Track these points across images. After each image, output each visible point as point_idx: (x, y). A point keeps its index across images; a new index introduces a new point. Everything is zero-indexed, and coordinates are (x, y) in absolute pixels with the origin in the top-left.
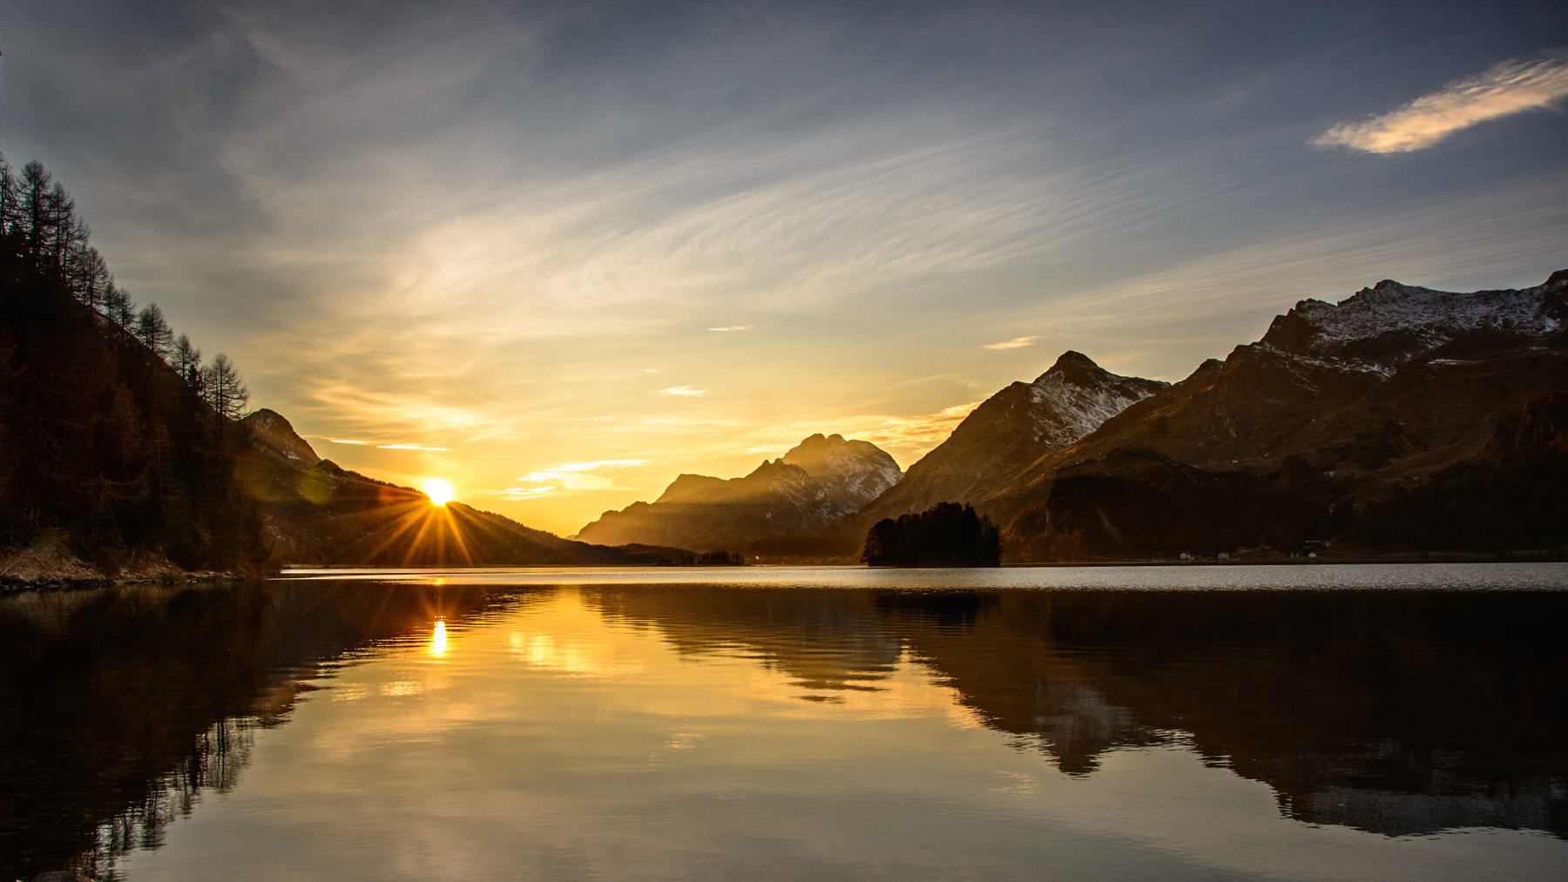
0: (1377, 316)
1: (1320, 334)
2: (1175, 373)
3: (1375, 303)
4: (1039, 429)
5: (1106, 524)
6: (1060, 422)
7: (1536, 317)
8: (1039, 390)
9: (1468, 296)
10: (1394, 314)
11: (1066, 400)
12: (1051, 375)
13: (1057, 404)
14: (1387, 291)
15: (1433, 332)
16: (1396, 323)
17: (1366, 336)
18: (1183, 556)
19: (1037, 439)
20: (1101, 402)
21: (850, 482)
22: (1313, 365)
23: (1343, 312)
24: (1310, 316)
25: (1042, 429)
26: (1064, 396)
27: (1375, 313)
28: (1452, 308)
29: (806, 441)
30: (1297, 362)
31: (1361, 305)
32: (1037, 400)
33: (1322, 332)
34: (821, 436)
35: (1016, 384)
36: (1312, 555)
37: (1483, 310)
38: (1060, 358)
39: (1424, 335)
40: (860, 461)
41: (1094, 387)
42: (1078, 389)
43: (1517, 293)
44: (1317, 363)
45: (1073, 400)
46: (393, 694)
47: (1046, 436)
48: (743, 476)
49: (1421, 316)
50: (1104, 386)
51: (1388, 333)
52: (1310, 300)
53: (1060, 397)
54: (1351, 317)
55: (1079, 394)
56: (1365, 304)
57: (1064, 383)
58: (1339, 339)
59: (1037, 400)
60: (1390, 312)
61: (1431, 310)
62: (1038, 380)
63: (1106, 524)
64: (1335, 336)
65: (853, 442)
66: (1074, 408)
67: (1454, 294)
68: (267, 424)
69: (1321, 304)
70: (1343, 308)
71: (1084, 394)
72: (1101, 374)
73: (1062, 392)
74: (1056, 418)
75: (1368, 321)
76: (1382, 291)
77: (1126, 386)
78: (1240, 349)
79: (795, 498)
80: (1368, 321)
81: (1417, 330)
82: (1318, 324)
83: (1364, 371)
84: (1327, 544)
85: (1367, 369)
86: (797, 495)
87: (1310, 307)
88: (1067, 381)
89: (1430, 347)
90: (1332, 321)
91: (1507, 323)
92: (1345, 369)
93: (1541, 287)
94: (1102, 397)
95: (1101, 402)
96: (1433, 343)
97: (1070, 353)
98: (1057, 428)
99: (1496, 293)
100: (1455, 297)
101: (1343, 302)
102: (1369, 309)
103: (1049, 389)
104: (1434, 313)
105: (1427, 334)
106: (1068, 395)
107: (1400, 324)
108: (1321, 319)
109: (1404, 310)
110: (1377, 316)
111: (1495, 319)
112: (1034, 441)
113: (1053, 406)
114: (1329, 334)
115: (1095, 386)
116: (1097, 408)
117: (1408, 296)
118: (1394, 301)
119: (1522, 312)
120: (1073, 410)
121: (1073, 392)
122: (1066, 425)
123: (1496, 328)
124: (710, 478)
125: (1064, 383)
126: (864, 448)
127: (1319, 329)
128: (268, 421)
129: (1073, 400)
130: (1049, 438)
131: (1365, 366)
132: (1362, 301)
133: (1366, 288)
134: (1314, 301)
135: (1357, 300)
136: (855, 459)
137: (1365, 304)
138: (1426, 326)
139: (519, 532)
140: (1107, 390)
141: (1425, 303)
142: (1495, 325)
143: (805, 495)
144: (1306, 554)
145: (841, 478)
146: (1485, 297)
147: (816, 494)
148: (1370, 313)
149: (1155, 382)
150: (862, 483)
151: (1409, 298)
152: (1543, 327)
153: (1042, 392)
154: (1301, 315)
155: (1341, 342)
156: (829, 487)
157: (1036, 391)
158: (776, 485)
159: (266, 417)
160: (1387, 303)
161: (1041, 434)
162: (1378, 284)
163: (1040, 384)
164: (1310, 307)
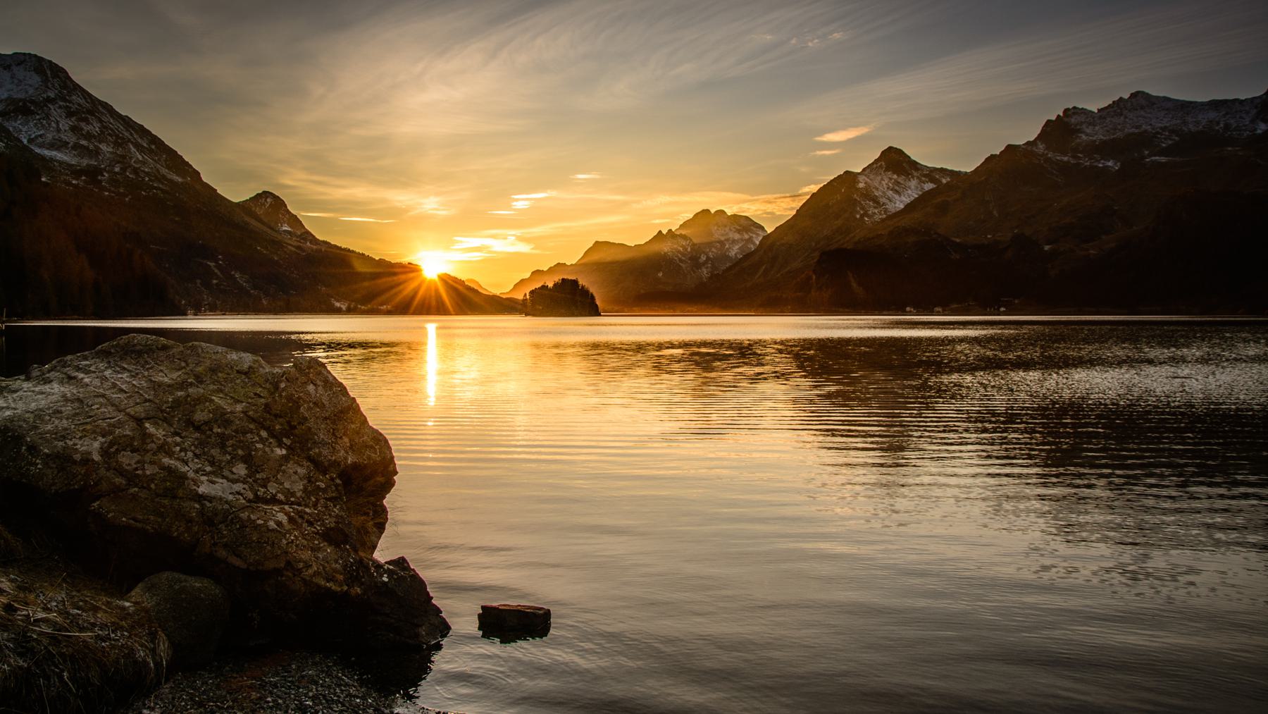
0: (1127, 120)
1: (1080, 135)
2: (968, 168)
3: (1127, 109)
4: (860, 208)
5: (854, 285)
6: (878, 203)
7: (1252, 121)
8: (864, 177)
9: (1202, 104)
10: (1140, 118)
11: (885, 185)
12: (875, 166)
13: (877, 189)
14: (1140, 100)
15: (1167, 133)
16: (1141, 126)
17: (1115, 136)
18: (908, 309)
19: (858, 216)
20: (913, 187)
21: (730, 248)
22: (1061, 161)
23: (1100, 117)
25: (863, 208)
26: (883, 182)
28: (1188, 114)
29: (696, 215)
30: (1050, 158)
31: (1115, 111)
32: (861, 185)
33: (1081, 133)
34: (708, 211)
35: (847, 172)
36: (1002, 309)
37: (1212, 115)
38: (883, 152)
39: (1159, 136)
40: (739, 231)
41: (908, 175)
42: (895, 176)
43: (1241, 102)
44: (1066, 159)
45: (890, 185)
46: (140, 585)
47: (866, 214)
48: (643, 243)
49: (1162, 120)
50: (915, 174)
51: (1133, 134)
52: (1074, 108)
53: (880, 183)
54: (1107, 121)
55: (896, 181)
56: (1119, 111)
57: (884, 171)
58: (1094, 138)
59: (861, 185)
60: (1137, 117)
61: (1171, 116)
62: (864, 170)
63: (854, 285)
64: (1091, 136)
65: (735, 216)
66: (891, 192)
67: (1191, 103)
68: (267, 203)
70: (1100, 114)
71: (899, 181)
72: (915, 165)
73: (882, 179)
74: (875, 200)
75: (1119, 124)
76: (1133, 100)
77: (932, 174)
78: (1009, 147)
79: (681, 260)
80: (1119, 124)
81: (1154, 131)
82: (1078, 127)
83: (1101, 165)
84: (1016, 301)
85: (1103, 164)
86: (683, 258)
87: (1074, 113)
88: (887, 170)
89: (1164, 145)
90: (1090, 124)
91: (1227, 127)
92: (1086, 164)
93: (1260, 97)
94: (913, 183)
95: (913, 187)
96: (1166, 142)
97: (890, 148)
98: (875, 208)
99: (1225, 102)
100: (1192, 105)
101: (1102, 109)
102: (1121, 115)
103: (872, 177)
104: (1172, 118)
105: (1162, 135)
106: (886, 182)
107: (1144, 126)
108: (1082, 122)
109: (1149, 115)
110: (1127, 120)
111: (1218, 123)
112: (856, 219)
114: (1087, 135)
115: (909, 174)
116: (910, 192)
117: (1155, 104)
118: (1142, 108)
119: (1241, 117)
120: (890, 193)
121: (891, 179)
122: (883, 205)
123: (1218, 130)
124: (619, 244)
125: (884, 171)
126: (742, 222)
127: (1079, 131)
128: (268, 200)
129: (890, 185)
130: (868, 216)
131: (1102, 161)
132: (1116, 108)
133: (1121, 98)
134: (1078, 108)
135: (1113, 107)
136: (734, 230)
137: (1119, 111)
139: (756, 213)
140: (918, 178)
141: (1167, 110)
142: (1217, 128)
143: (690, 259)
144: (998, 309)
145: (721, 242)
146: (1215, 105)
147: (700, 258)
148: (1122, 118)
149: (956, 172)
150: (740, 248)
151: (1155, 106)
152: (1256, 130)
153: (866, 179)
154: (1066, 119)
155: (1095, 141)
156: (713, 252)
157: (861, 178)
158: (666, 247)
159: (267, 197)
160: (1137, 110)
162: (1132, 94)
163: (866, 172)
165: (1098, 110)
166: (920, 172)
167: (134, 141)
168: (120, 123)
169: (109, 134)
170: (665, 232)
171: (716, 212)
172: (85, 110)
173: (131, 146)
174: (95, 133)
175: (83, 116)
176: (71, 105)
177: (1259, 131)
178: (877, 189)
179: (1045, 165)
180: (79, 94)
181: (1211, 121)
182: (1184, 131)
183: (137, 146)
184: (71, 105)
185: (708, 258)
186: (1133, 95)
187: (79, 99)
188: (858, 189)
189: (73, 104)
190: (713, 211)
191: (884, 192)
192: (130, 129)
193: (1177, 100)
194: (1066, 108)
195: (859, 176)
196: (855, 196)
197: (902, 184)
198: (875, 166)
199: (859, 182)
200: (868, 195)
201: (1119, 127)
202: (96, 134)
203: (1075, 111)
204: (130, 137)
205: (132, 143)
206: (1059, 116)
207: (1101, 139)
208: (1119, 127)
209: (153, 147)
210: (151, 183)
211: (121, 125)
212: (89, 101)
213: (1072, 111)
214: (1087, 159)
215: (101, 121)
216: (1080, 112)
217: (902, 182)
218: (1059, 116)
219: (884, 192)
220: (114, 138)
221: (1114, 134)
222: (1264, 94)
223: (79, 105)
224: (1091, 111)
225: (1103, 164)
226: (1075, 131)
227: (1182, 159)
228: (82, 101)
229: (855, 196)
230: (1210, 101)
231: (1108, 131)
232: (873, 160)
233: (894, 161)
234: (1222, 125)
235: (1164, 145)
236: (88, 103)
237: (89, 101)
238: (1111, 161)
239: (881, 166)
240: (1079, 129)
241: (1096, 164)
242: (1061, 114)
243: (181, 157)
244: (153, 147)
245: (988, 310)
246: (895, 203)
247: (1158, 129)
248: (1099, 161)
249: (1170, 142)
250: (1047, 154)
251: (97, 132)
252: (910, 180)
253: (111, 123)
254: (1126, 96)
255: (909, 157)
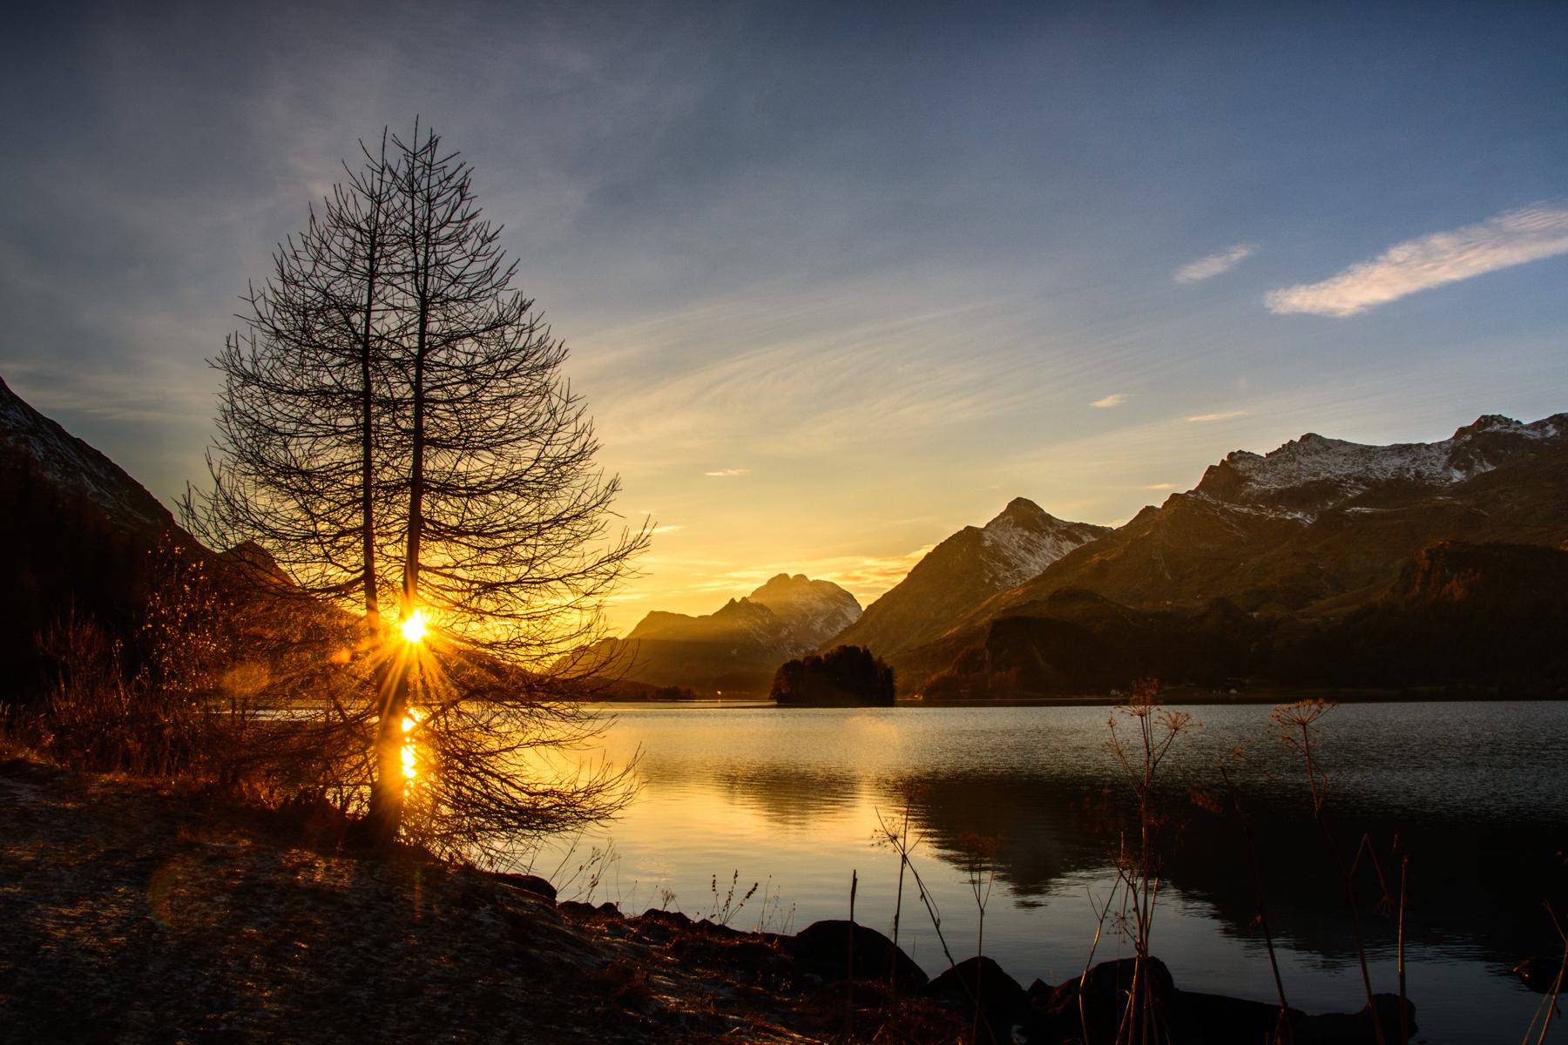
0: (1302, 466)
1: (1250, 483)
6: (1009, 564)
7: (1445, 469)
8: (989, 533)
9: (1384, 449)
12: (1001, 521)
15: (1352, 482)
16: (1319, 473)
19: (987, 581)
20: (1048, 546)
22: (1241, 513)
24: (1240, 466)
27: (1300, 463)
28: (1370, 460)
31: (1287, 456)
32: (987, 543)
33: (1251, 481)
34: (785, 576)
37: (1397, 461)
39: (1344, 485)
41: (1042, 532)
42: (1027, 533)
43: (1428, 447)
44: (1245, 510)
47: (995, 578)
49: (1342, 467)
50: (1050, 530)
51: (1311, 482)
52: (1240, 452)
55: (1028, 538)
57: (1013, 527)
58: (1267, 488)
59: (987, 543)
60: (1313, 463)
62: (988, 525)
66: (1023, 551)
67: (1371, 447)
69: (1250, 456)
70: (1270, 459)
71: (1032, 538)
72: (1049, 519)
73: (1012, 537)
75: (1293, 471)
79: (760, 636)
82: (1247, 474)
83: (1288, 518)
84: (1247, 681)
85: (1291, 516)
86: (762, 632)
87: (1240, 458)
88: (1016, 525)
89: (1350, 495)
90: (1260, 471)
92: (1270, 516)
93: (1448, 442)
95: (1048, 546)
98: (1007, 570)
99: (1409, 447)
101: (1271, 453)
102: (1294, 460)
103: (999, 533)
107: (1322, 474)
108: (1250, 469)
109: (1326, 461)
110: (1302, 466)
111: (1408, 470)
112: (985, 582)
113: (1003, 549)
114: (1258, 483)
116: (1045, 551)
117: (1330, 448)
118: (1317, 452)
119: (1432, 464)
121: (1022, 536)
124: (679, 615)
127: (1249, 479)
130: (999, 580)
135: (1283, 452)
137: (1291, 456)
138: (1345, 476)
140: (1054, 535)
141: (1345, 455)
142: (1408, 476)
147: (780, 632)
152: (1451, 478)
155: (1269, 491)
157: (986, 535)
158: (740, 623)
161: (991, 576)
162: (1303, 437)
164: (1240, 458)
165: (1267, 454)
166: (1056, 528)
167: (89, 471)
168: (70, 447)
169: (56, 461)
170: (738, 600)
171: (795, 576)
172: (24, 428)
173: (85, 477)
174: (37, 458)
175: (23, 436)
176: (7, 422)
177: (1455, 480)
178: (1006, 548)
179: (1222, 517)
180: (19, 408)
181: (1400, 469)
182: (1371, 479)
183: (92, 476)
184: (7, 422)
185: (790, 633)
186: (1307, 438)
187: (17, 414)
188: (983, 548)
189: (10, 420)
190: (791, 576)
191: (1014, 552)
192: (84, 456)
193: (1355, 445)
194: (1230, 452)
195: (984, 532)
196: (981, 556)
197: (1035, 542)
198: (1001, 521)
199: (985, 539)
200: (995, 553)
201: (1294, 474)
202: (39, 460)
203: (1241, 455)
204: (82, 465)
205: (86, 473)
206: (1223, 461)
207: (1275, 489)
208: (1294, 474)
209: (113, 479)
210: (114, 523)
211: (72, 449)
212: (31, 417)
213: (1238, 455)
214: (1270, 510)
215: (45, 444)
216: (1246, 456)
217: (1035, 540)
218: (1223, 461)
219: (1014, 552)
220: (62, 465)
221: (1289, 483)
222: (1452, 439)
223: (18, 422)
224: (1258, 456)
225: (1291, 516)
226: (1243, 480)
227: (1388, 510)
228: (22, 418)
229: (981, 556)
230: (1393, 446)
231: (1282, 479)
232: (998, 514)
233: (1024, 514)
234: (1413, 473)
235: (1350, 495)
236: (29, 419)
237: (31, 417)
238: (1299, 513)
239: (1008, 520)
240: (1249, 477)
241: (1282, 516)
242: (1226, 459)
243: (149, 493)
244: (113, 479)
245: (1214, 692)
246: (1029, 565)
247: (1342, 477)
248: (1285, 513)
249: (1358, 493)
250: (1223, 505)
251: (40, 457)
252: (1044, 538)
253: (58, 447)
254: (1297, 439)
255: (1042, 510)
